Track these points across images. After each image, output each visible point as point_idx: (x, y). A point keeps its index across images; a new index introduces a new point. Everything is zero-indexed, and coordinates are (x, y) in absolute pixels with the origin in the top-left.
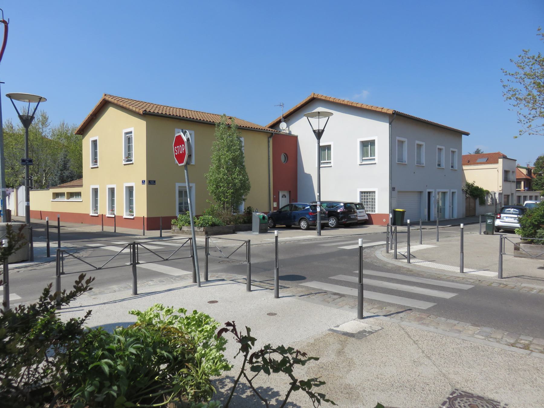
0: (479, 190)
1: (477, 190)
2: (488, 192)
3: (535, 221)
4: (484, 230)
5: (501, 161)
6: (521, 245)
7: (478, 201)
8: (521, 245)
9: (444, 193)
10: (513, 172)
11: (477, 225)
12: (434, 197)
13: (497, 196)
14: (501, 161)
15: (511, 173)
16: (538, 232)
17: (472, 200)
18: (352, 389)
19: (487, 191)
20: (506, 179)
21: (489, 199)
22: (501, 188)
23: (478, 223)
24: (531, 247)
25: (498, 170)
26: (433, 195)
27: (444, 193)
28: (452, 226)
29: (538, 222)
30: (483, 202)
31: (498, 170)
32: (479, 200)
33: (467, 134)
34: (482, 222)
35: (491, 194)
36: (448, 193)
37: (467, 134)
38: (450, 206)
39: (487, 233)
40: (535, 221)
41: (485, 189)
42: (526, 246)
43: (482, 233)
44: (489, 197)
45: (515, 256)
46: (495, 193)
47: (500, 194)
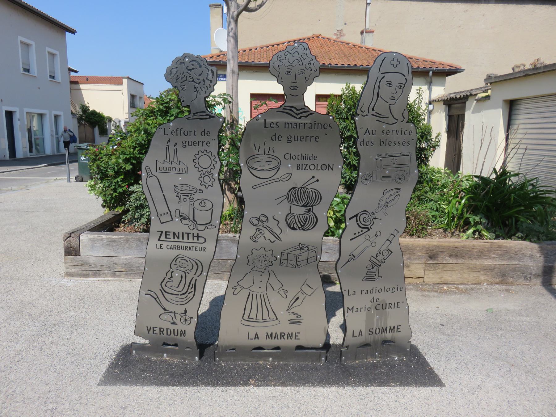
0: (97, 116)
1: (95, 115)
2: (110, 120)
3: (126, 161)
4: (75, 173)
5: (125, 81)
6: (85, 237)
7: (97, 130)
8: (85, 237)
9: (41, 116)
10: (140, 98)
11: (64, 167)
12: (19, 120)
13: (122, 124)
14: (125, 81)
15: (138, 98)
16: (133, 192)
17: (89, 129)
18: (51, 290)
19: (109, 117)
20: (132, 105)
21: (113, 128)
22: (128, 115)
23: (65, 163)
24: (111, 243)
25: (122, 93)
26: (16, 117)
27: (41, 116)
28: (49, 165)
29: (132, 164)
30: (104, 132)
31: (122, 93)
32: (99, 128)
33: (73, 32)
34: (70, 162)
35: (115, 122)
36: (48, 116)
37: (73, 32)
38: (52, 136)
39: (80, 179)
40: (126, 161)
41: (106, 114)
42: (96, 240)
43: (73, 178)
44: (113, 125)
45: (68, 275)
46: (120, 122)
47: (125, 122)
